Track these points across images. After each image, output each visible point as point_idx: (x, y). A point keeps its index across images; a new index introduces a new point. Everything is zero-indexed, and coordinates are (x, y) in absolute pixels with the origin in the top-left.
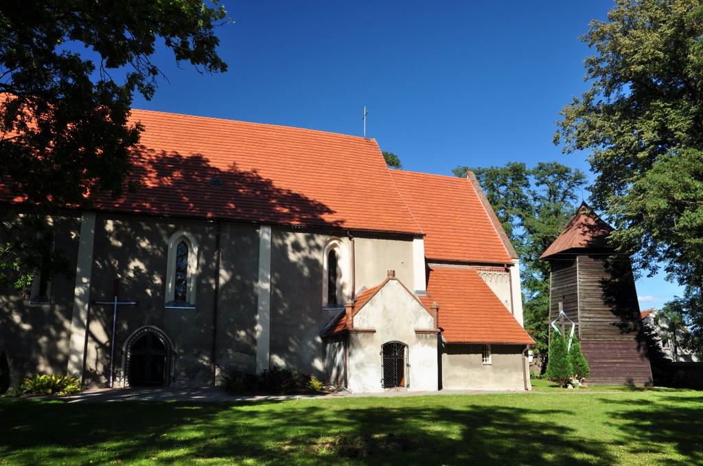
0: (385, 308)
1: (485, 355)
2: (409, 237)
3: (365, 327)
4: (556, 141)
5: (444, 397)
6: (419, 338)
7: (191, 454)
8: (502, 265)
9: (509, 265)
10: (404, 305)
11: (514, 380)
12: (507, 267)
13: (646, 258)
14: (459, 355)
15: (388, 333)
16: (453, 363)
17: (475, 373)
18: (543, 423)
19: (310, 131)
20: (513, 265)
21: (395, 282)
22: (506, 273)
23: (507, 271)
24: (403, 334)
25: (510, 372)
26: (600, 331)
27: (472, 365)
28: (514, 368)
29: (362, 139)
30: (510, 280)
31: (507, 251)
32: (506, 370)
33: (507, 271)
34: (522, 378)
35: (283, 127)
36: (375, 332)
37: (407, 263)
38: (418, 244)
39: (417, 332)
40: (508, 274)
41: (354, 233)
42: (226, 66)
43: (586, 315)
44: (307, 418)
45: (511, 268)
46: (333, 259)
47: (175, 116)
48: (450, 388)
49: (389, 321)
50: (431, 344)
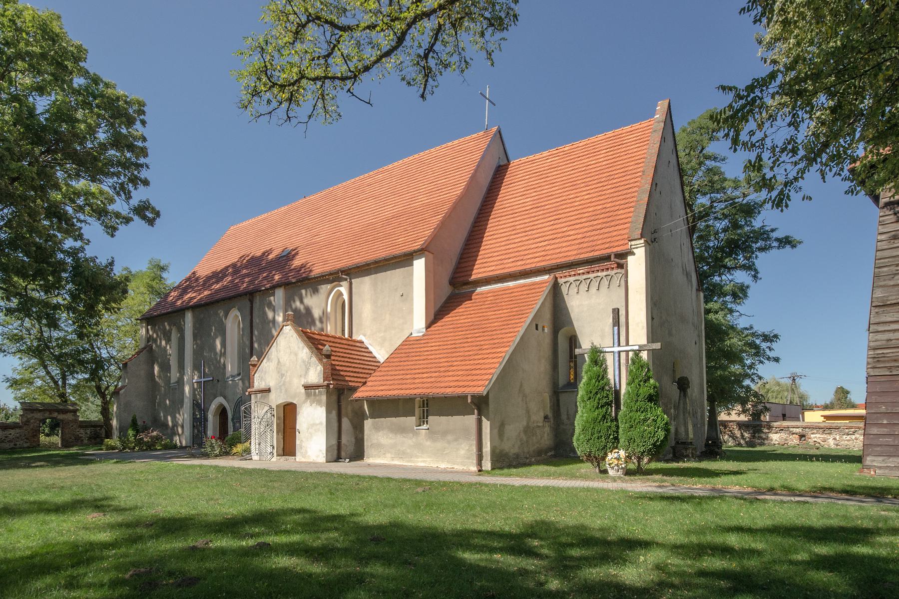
0: (279, 362)
2: (405, 260)
5: (363, 484)
7: (682, 546)
8: (607, 258)
10: (296, 355)
11: (462, 452)
12: (620, 259)
13: (85, 137)
14: (393, 419)
17: (406, 442)
18: (825, 556)
22: (619, 270)
23: (620, 266)
24: (296, 394)
27: (402, 430)
30: (627, 277)
32: (450, 437)
37: (406, 296)
39: (307, 387)
40: (623, 271)
41: (334, 277)
49: (283, 375)
50: (319, 403)
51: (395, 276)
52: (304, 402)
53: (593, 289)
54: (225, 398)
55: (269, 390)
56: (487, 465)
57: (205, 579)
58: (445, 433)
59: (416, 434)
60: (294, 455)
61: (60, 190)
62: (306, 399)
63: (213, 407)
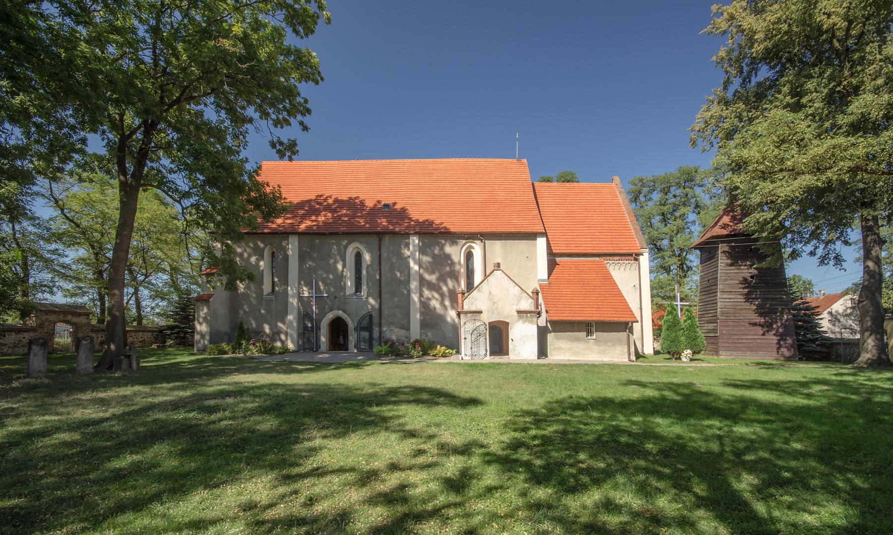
1: (589, 333)
2: (532, 236)
3: (474, 308)
4: (694, 143)
5: (551, 366)
6: (520, 317)
8: (631, 255)
9: (638, 255)
10: (508, 290)
11: (617, 352)
12: (636, 257)
15: (493, 313)
16: (558, 339)
19: (471, 160)
20: (642, 254)
21: (499, 272)
23: (636, 260)
24: (506, 311)
25: (613, 345)
26: (741, 310)
27: (577, 340)
28: (619, 342)
29: (515, 160)
30: (639, 268)
31: (636, 240)
32: (609, 344)
33: (636, 260)
34: (626, 350)
35: (449, 160)
36: (481, 312)
37: (531, 257)
38: (541, 242)
39: (519, 312)
42: (303, 130)
43: (725, 296)
44: (833, 393)
45: (641, 257)
46: (469, 256)
47: (370, 162)
48: (554, 357)
49: (494, 303)
51: (523, 244)
52: (517, 321)
53: (622, 269)
54: (344, 311)
55: (481, 312)
56: (633, 358)
57: (583, 463)
58: (606, 342)
59: (586, 342)
60: (508, 354)
61: (87, 42)
62: (518, 320)
63: (330, 316)
